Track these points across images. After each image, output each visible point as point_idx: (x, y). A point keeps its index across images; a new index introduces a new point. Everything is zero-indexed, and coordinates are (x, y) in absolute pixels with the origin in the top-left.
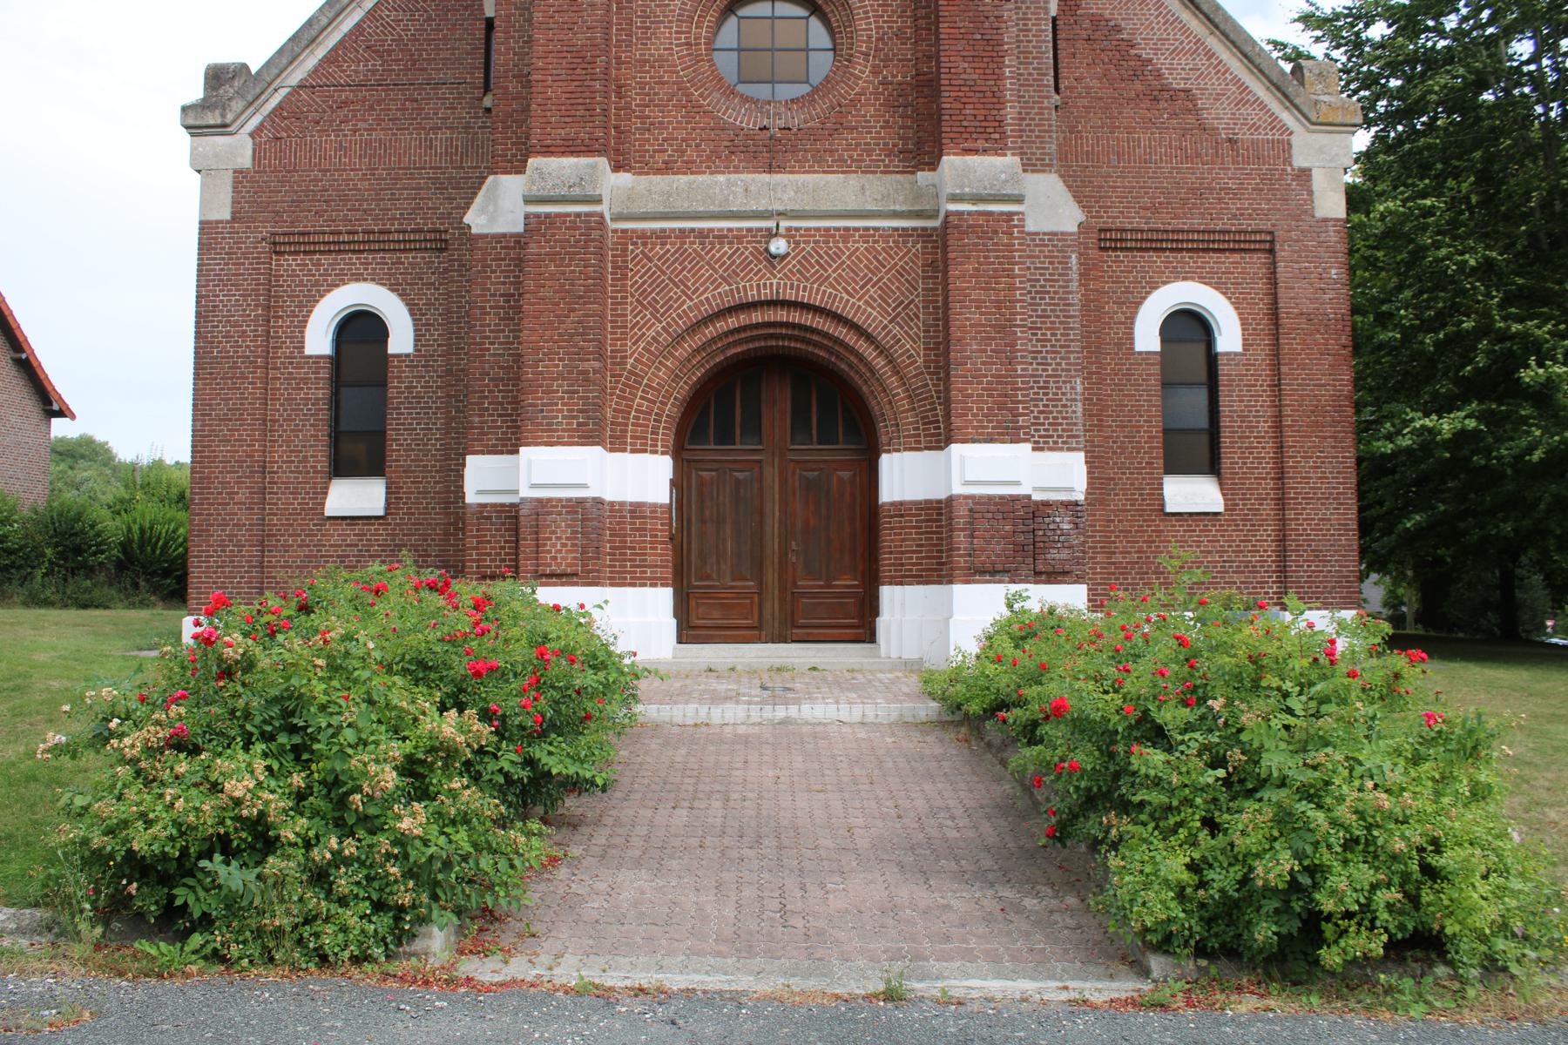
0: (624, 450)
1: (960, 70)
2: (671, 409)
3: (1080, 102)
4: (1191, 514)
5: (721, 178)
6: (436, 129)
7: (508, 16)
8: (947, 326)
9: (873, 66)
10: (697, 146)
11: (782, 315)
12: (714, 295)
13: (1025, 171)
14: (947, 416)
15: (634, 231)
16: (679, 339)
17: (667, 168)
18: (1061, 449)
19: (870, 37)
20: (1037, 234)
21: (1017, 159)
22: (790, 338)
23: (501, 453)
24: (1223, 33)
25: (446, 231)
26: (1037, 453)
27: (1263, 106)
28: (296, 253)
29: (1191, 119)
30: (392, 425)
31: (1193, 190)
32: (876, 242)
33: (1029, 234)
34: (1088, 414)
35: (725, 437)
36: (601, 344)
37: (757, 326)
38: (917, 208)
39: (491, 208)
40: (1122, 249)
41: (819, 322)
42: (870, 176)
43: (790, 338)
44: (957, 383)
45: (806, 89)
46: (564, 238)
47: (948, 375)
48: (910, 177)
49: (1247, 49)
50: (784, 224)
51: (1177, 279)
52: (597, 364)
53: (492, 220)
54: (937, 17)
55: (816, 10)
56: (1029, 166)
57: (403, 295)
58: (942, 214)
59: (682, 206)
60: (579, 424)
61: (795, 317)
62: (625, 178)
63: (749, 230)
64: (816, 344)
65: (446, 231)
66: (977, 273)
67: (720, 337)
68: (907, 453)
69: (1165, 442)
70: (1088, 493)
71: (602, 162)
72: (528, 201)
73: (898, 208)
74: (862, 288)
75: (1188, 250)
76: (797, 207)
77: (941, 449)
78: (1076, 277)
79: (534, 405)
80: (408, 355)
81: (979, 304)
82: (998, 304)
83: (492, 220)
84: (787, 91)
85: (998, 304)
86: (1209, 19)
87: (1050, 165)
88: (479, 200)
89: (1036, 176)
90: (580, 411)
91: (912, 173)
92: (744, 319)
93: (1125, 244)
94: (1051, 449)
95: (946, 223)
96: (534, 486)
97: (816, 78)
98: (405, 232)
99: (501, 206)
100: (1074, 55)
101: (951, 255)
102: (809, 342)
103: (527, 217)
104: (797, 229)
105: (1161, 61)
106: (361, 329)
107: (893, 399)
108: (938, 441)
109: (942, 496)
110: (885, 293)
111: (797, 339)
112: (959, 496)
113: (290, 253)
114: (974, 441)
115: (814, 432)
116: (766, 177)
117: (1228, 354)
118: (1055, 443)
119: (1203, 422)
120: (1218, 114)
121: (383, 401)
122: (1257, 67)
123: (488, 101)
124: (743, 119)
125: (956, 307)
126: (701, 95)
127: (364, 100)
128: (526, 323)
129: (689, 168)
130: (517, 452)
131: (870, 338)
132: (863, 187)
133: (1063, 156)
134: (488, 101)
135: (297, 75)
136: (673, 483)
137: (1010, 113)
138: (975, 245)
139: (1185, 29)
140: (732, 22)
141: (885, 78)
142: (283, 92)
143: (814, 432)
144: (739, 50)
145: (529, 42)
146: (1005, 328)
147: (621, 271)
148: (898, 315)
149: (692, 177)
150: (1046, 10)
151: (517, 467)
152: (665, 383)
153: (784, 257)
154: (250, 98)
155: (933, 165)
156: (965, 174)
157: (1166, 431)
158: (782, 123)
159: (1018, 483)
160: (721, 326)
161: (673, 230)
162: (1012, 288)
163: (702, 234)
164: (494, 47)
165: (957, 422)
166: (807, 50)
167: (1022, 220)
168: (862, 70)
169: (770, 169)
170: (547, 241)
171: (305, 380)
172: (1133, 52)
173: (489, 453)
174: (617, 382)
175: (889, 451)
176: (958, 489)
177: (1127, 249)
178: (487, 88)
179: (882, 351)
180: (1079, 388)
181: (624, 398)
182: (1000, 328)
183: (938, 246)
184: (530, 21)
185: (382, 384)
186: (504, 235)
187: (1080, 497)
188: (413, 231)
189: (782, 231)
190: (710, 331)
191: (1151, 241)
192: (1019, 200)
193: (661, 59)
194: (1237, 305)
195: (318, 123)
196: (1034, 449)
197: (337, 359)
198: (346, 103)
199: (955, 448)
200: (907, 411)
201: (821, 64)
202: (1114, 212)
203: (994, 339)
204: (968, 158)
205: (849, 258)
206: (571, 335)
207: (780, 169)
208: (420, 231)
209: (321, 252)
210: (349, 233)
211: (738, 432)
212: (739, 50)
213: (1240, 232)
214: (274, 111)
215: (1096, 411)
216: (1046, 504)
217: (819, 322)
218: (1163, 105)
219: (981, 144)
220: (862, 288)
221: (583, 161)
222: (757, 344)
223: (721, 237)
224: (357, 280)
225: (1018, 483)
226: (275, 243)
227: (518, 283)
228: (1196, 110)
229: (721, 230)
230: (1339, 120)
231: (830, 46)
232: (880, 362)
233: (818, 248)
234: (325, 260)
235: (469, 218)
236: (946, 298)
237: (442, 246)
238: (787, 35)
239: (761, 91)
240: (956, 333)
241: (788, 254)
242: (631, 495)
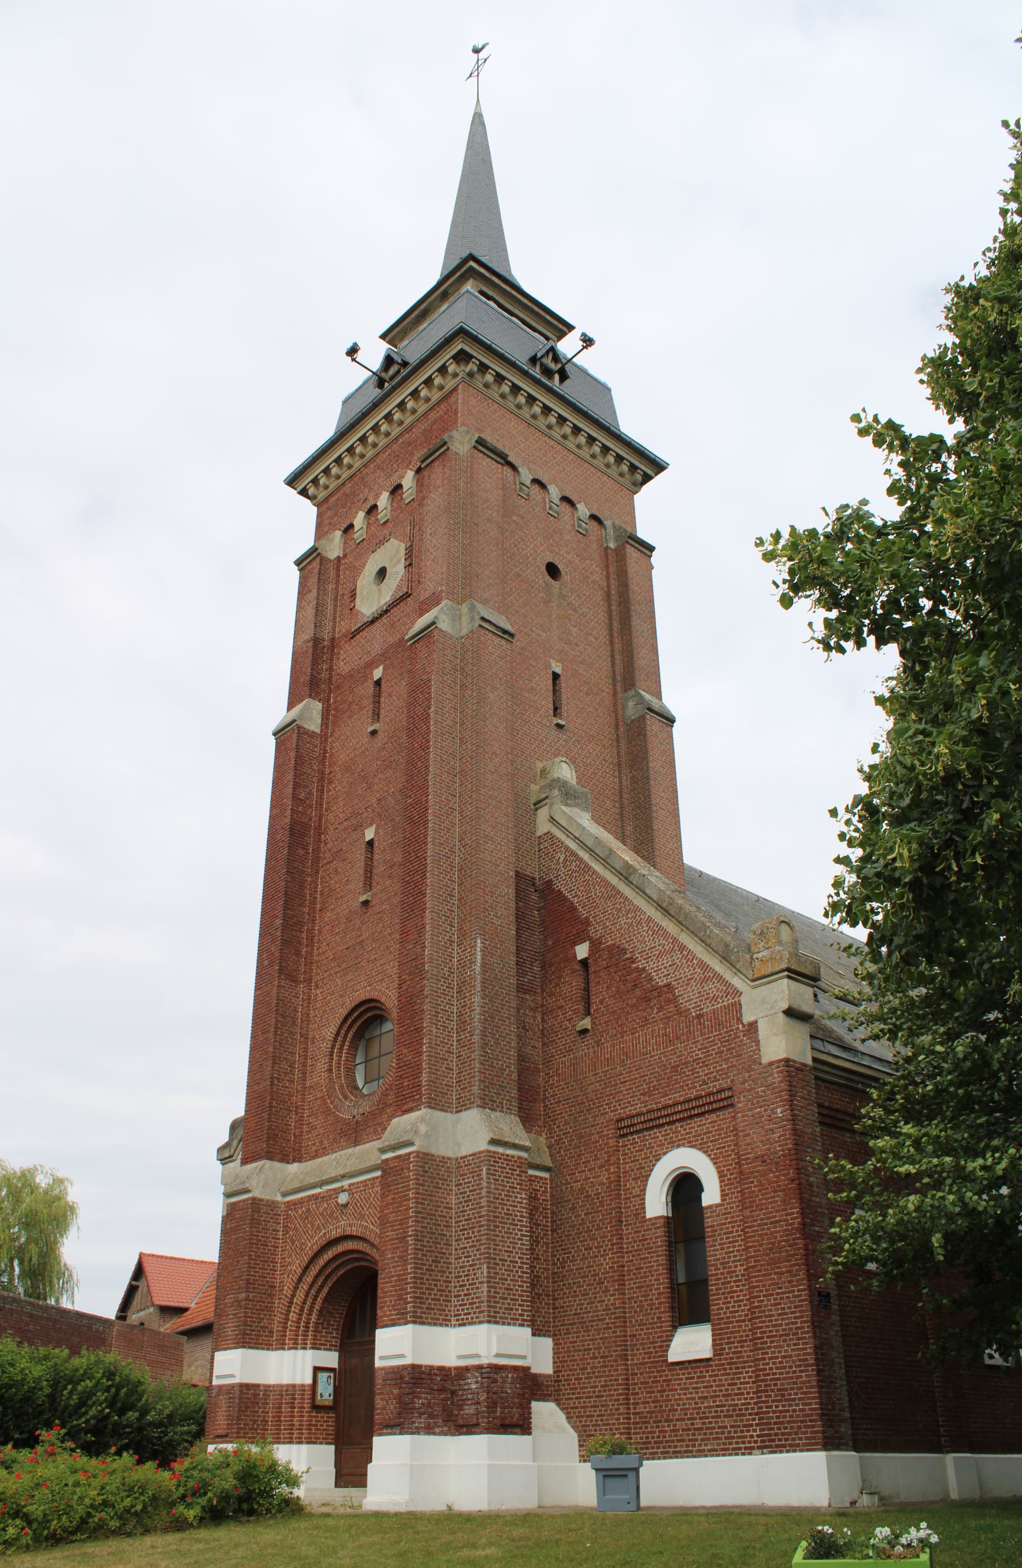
4: (690, 1362)
17: (316, 1156)
18: (474, 1323)
29: (672, 1008)
94: (470, 1324)
158: (361, 1111)
163: (315, 1197)
191: (651, 1120)
194: (715, 1161)
219: (411, 1105)
225: (402, 1356)
230: (770, 970)
242: (286, 1379)
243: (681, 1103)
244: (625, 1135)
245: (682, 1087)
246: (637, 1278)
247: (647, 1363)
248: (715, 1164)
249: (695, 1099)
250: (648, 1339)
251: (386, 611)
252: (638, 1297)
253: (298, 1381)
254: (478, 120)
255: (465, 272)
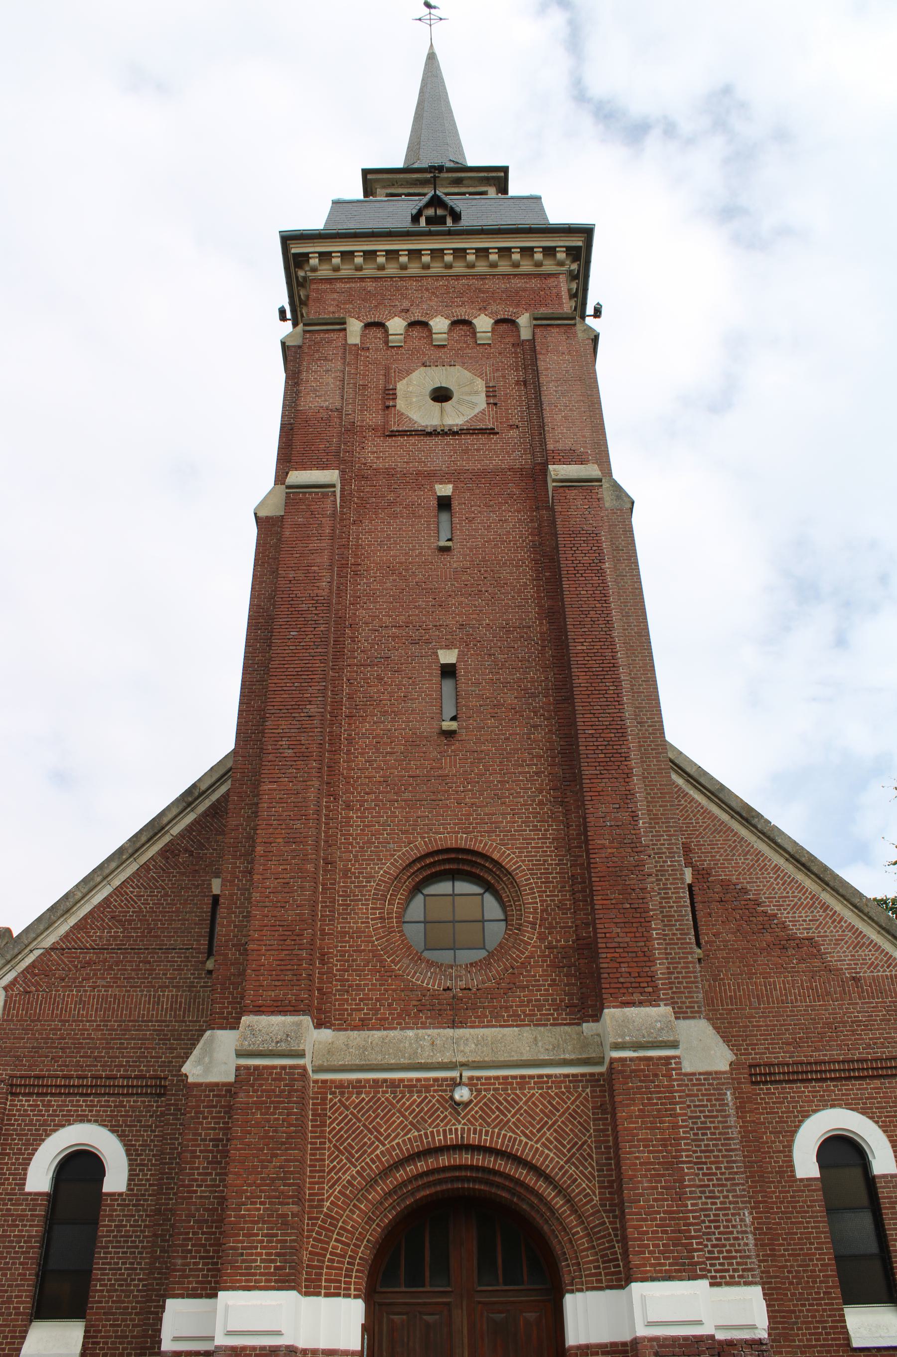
0: (318, 1294)
1: (614, 935)
2: (364, 1252)
3: (720, 954)
5: (410, 1033)
6: (163, 987)
7: (231, 895)
8: (618, 1166)
9: (540, 933)
10: (390, 1005)
11: (467, 1158)
12: (404, 1140)
13: (677, 1018)
14: (626, 1253)
15: (332, 1081)
16: (372, 1183)
17: (363, 1025)
18: (738, 1284)
19: (535, 909)
20: (694, 1074)
21: (669, 1009)
22: (475, 1180)
23: (200, 1296)
24: (833, 889)
25: (165, 1078)
26: (716, 1289)
27: (877, 947)
28: (30, 1094)
29: (817, 963)
30: (98, 1264)
31: (828, 1025)
32: (549, 1088)
33: (686, 1074)
34: (760, 1244)
35: (415, 1279)
36: (300, 1188)
37: (444, 1169)
38: (584, 1056)
39: (207, 1059)
40: (772, 1082)
41: (500, 1165)
42: (542, 1029)
43: (475, 1180)
44: (632, 1220)
45: (483, 954)
46: (269, 1087)
47: (623, 1213)
48: (577, 1028)
49: (856, 901)
50: (467, 1074)
51: (825, 1107)
52: (295, 1208)
53: (207, 1070)
54: (592, 891)
55: (489, 888)
56: (680, 1014)
57: (122, 1137)
58: (607, 1061)
59: (376, 1058)
60: (276, 1268)
61: (479, 1160)
62: (326, 1034)
63: (436, 1080)
64: (498, 1186)
65: (165, 1078)
66: (642, 1114)
67: (410, 1180)
68: (590, 1294)
69: (839, 1270)
70: (770, 1328)
71: (306, 1020)
72: (239, 1054)
73: (567, 1056)
74: (539, 1131)
75: (832, 1079)
76: (478, 1059)
77: (622, 1287)
78: (732, 1112)
79: (234, 1248)
80: (121, 1194)
81: (646, 1142)
82: (664, 1142)
83: (207, 1070)
84: (467, 956)
85: (664, 1142)
86: (820, 878)
87: (699, 1012)
88: (196, 1052)
89: (688, 1022)
90: (278, 1254)
91: (579, 1024)
92: (431, 1162)
93: (775, 1081)
94: (728, 1284)
95: (611, 1068)
96: (230, 1333)
97: (491, 944)
98: (128, 1078)
99: (215, 1059)
100: (710, 914)
101: (618, 1098)
102: (492, 1184)
103: (238, 1068)
104: (479, 1078)
105: (785, 915)
106: (81, 1167)
107: (575, 1239)
108: (619, 1280)
109: (627, 1338)
110: (560, 1134)
111: (480, 1181)
112: (644, 1338)
113: (25, 1095)
114: (653, 1279)
115: (500, 1272)
116: (449, 1032)
117: (884, 1176)
118: (732, 1277)
119: (873, 1247)
120: (840, 956)
121: (92, 1239)
122: (866, 915)
123: (210, 965)
124: (428, 981)
125: (626, 1147)
126: (393, 961)
127: (105, 960)
128: (233, 1168)
129: (383, 1024)
130: (216, 1296)
131: (548, 1178)
132: (535, 1039)
133: (710, 1001)
134: (210, 965)
135: (50, 939)
136: (365, 1328)
137: (660, 969)
138: (637, 1087)
139: (801, 888)
140: (419, 898)
141: (550, 942)
142: (37, 953)
143: (500, 1272)
144: (425, 922)
145: (248, 916)
146: (672, 1165)
147: (320, 1118)
148: (573, 1155)
149: (385, 1033)
150: (683, 880)
151: (215, 1311)
152: (357, 1227)
153: (467, 1104)
154: (9, 957)
155: (596, 1017)
156: (625, 1023)
157: (837, 1258)
158: (462, 984)
159: (699, 1323)
160: (411, 1169)
161: (368, 1081)
162: (676, 1127)
163: (394, 1084)
164: (218, 920)
165: (635, 1260)
166: (483, 921)
167: (680, 1063)
168: (531, 937)
169: (453, 1025)
170: (255, 1091)
171: (22, 1217)
172: (760, 909)
173: (190, 1296)
174: (314, 1225)
175: (572, 1291)
176: (642, 1331)
177: (776, 1082)
178: (210, 953)
179: (561, 1191)
180: (748, 1219)
181: (320, 1241)
182: (668, 1165)
183: (607, 1090)
184: (249, 899)
185: (94, 1222)
186: (217, 1084)
187: (764, 1335)
188: (137, 1077)
189: (465, 1080)
190: (400, 1175)
191: (797, 1073)
192: (674, 1045)
193: (359, 931)
195: (63, 979)
196: (712, 1285)
197: (54, 1197)
198: (89, 963)
199: (636, 1288)
200: (587, 1249)
201: (496, 932)
202: (761, 1048)
203: (663, 1175)
204: (626, 1010)
205: (526, 1103)
206: (273, 1179)
207: (462, 1024)
208: (143, 1077)
209: (52, 1095)
210: (79, 1077)
211: (427, 1274)
212: (425, 922)
213: (876, 1060)
214: (27, 969)
215: (767, 1240)
216: (730, 1343)
217: (500, 1165)
218: (791, 952)
219: (636, 997)
220: (539, 1131)
221: (290, 1019)
222: (444, 1187)
223: (411, 1086)
224: (82, 1121)
226: (12, 1085)
227: (227, 1129)
228: (820, 955)
229: (411, 1080)
231: (502, 917)
232: (559, 1202)
233: (498, 1095)
234: (55, 1101)
235: (186, 1069)
236: (616, 1139)
237: (161, 1092)
238: (466, 909)
239: (445, 957)
240: (627, 1172)
241: (471, 1101)
243: (839, 1062)
244: (756, 1083)
245: (840, 1045)
246: (789, 1244)
247: (815, 1346)
248: (885, 1131)
249: (857, 1061)
250: (814, 1317)
251: (455, 433)
252: (792, 1266)
253: (342, 1346)
254: (432, 57)
255: (493, 178)
